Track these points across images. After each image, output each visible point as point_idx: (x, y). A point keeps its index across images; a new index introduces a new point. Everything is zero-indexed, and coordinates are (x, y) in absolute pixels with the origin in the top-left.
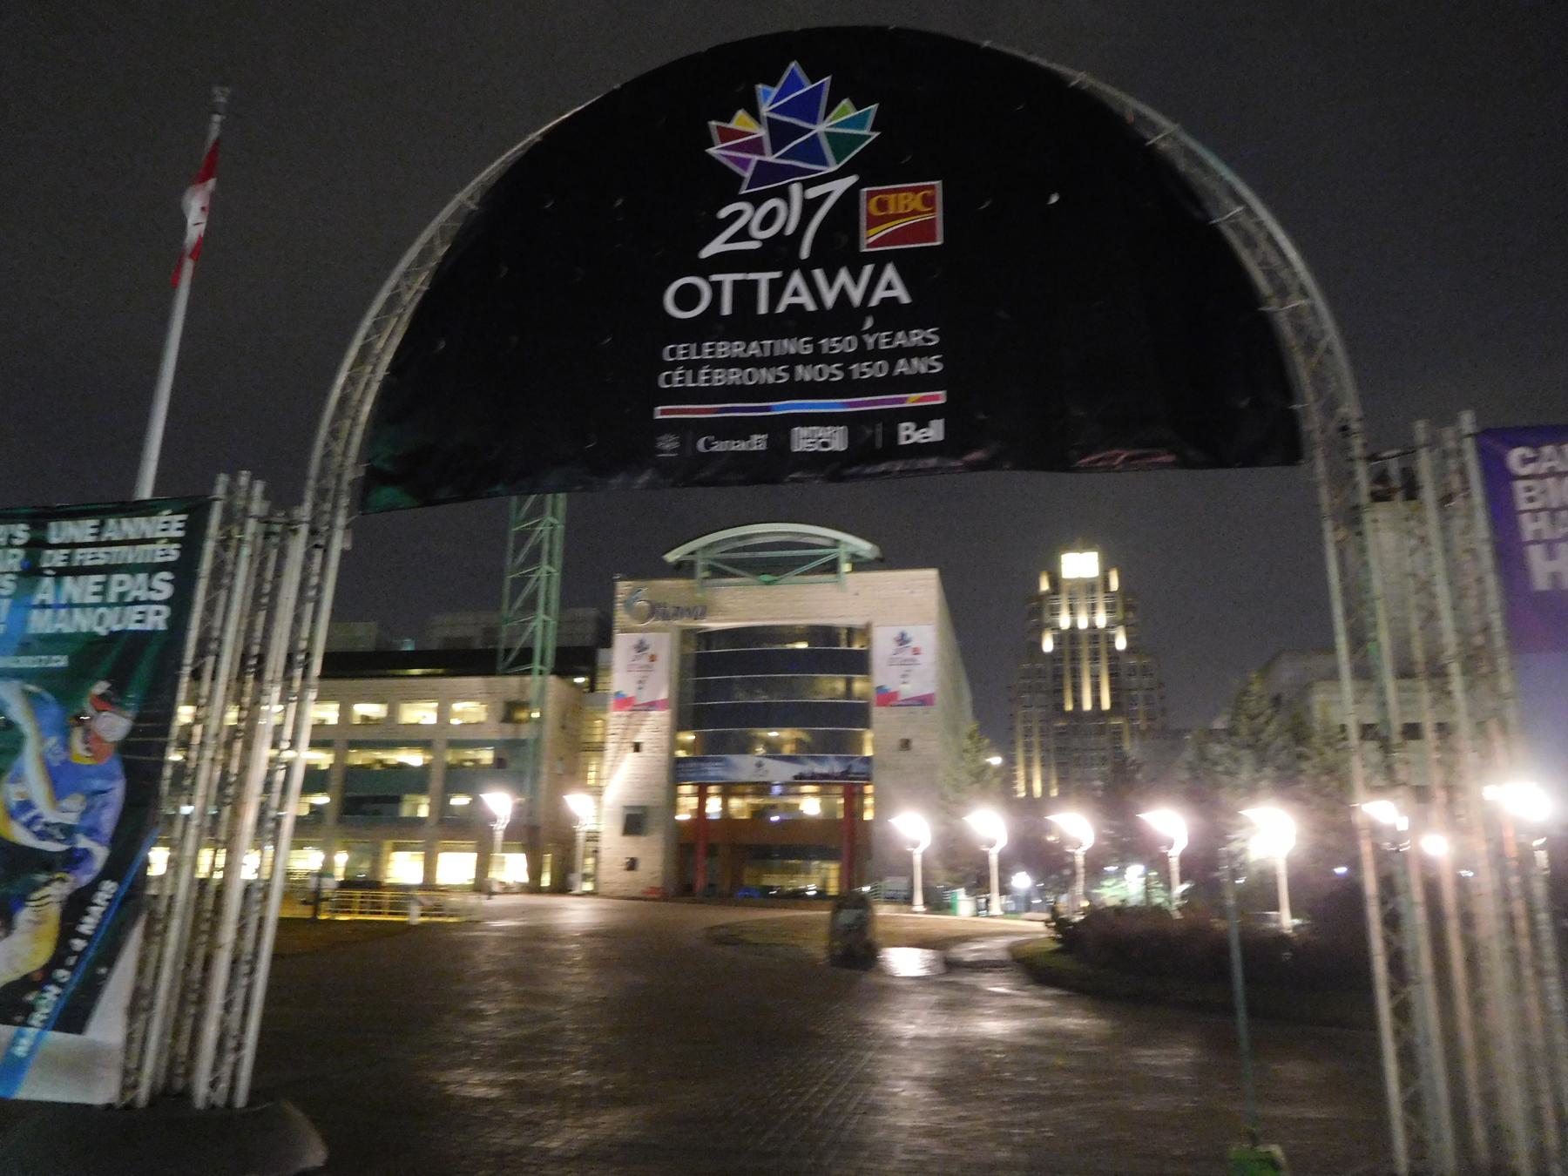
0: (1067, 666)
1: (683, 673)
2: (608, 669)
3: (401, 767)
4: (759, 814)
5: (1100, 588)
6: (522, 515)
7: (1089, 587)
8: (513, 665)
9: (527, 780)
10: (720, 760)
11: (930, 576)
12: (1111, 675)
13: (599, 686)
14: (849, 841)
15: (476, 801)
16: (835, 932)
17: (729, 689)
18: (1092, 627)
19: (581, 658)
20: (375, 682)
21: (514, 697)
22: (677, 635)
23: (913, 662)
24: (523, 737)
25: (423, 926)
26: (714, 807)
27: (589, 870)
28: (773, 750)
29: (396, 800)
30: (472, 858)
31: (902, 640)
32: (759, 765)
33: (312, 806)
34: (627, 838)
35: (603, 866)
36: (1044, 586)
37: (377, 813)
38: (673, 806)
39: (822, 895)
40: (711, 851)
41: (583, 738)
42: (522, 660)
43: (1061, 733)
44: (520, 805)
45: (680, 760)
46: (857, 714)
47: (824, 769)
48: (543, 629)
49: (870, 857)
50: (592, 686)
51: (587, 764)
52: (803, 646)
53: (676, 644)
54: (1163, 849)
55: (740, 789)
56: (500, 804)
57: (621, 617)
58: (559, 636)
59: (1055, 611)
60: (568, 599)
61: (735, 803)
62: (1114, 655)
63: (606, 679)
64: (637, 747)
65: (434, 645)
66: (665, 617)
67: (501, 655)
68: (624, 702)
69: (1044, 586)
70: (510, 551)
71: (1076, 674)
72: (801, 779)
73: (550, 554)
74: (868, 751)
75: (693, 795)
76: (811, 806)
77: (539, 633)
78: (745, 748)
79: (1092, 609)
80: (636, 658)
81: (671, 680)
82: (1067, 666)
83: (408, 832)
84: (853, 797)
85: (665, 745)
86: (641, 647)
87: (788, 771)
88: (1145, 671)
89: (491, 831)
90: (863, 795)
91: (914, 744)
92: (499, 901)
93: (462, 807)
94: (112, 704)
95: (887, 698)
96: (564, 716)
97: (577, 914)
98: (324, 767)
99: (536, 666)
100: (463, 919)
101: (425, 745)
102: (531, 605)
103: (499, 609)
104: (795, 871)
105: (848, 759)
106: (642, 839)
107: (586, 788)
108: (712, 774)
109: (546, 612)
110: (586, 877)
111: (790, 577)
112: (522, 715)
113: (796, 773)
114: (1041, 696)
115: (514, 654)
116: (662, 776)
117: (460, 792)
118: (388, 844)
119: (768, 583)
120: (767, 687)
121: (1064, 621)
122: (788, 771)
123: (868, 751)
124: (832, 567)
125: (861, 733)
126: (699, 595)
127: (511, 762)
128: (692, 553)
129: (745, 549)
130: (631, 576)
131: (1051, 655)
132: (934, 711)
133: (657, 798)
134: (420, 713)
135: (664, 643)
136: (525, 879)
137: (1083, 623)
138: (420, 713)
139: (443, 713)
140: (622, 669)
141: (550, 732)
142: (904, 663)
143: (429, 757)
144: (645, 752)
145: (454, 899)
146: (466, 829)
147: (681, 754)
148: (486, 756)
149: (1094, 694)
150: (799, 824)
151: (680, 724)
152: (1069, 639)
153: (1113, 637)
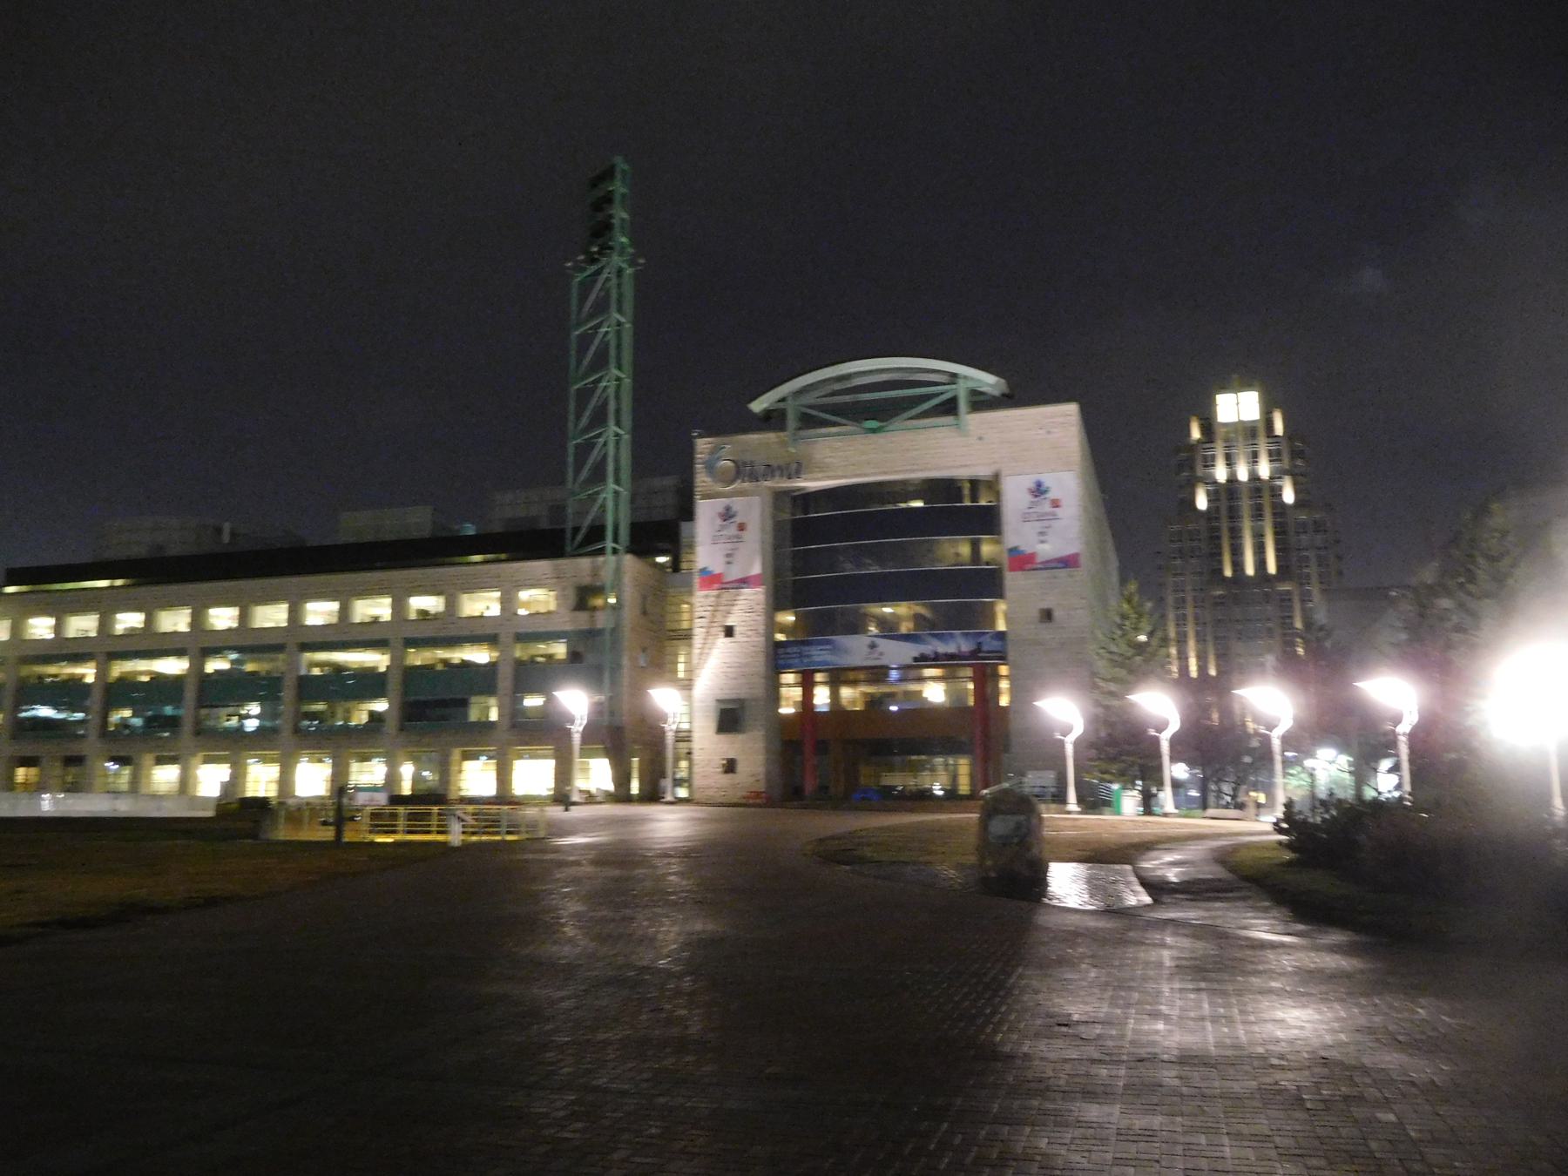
0: (1224, 525)
1: (777, 547)
2: (691, 546)
3: (466, 665)
4: (874, 703)
6: (583, 369)
7: (1249, 431)
8: (581, 545)
9: (607, 675)
10: (828, 642)
11: (1069, 412)
12: (1276, 533)
13: (684, 565)
14: (983, 731)
15: (550, 700)
16: (986, 845)
17: (834, 559)
18: (1254, 477)
19: (660, 534)
21: (587, 581)
22: (769, 499)
23: (1055, 517)
24: (599, 626)
25: (466, 848)
26: (822, 697)
27: (682, 774)
28: (889, 629)
29: (464, 703)
30: (550, 764)
31: (1039, 490)
32: (873, 646)
33: (372, 714)
34: (722, 737)
35: (696, 769)
36: (1196, 434)
37: (444, 718)
38: (774, 698)
39: (952, 795)
40: (821, 747)
41: (670, 626)
43: (1219, 603)
44: (599, 704)
45: (779, 644)
46: (987, 582)
47: (950, 648)
48: (614, 501)
49: (1006, 748)
50: (675, 566)
51: (676, 655)
52: (919, 504)
53: (769, 510)
54: (1152, 732)
55: (851, 675)
56: (576, 702)
57: (702, 480)
58: (634, 509)
59: (1209, 462)
60: (642, 467)
61: (846, 693)
62: (1280, 508)
63: (691, 557)
65: (497, 528)
66: (754, 477)
67: (569, 535)
69: (1196, 434)
70: (572, 417)
71: (1236, 534)
72: (924, 660)
73: (618, 411)
74: (1001, 626)
76: (935, 693)
77: (610, 505)
78: (856, 627)
79: (1254, 457)
80: (722, 528)
82: (1224, 525)
83: (477, 738)
84: (986, 680)
85: (762, 629)
86: (727, 515)
87: (906, 652)
88: (1318, 527)
89: (568, 733)
90: (996, 677)
91: (1057, 614)
92: (576, 812)
93: (536, 708)
95: (1022, 561)
96: (644, 598)
97: (668, 825)
98: (382, 669)
99: (609, 544)
100: (524, 836)
101: (491, 640)
102: (598, 475)
103: (563, 482)
104: (915, 768)
106: (740, 737)
107: (674, 680)
108: (817, 659)
109: (617, 481)
110: (678, 783)
111: (897, 423)
112: (599, 602)
113: (916, 654)
115: (583, 531)
117: (533, 691)
118: (456, 753)
119: (874, 431)
120: (877, 554)
121: (1221, 473)
122: (906, 652)
123: (1001, 626)
124: (949, 408)
125: (992, 605)
127: (589, 655)
128: (783, 400)
129: (834, 394)
130: (709, 432)
132: (1081, 574)
133: (759, 691)
134: (483, 604)
135: (753, 508)
136: (610, 787)
137: (1243, 474)
138: (483, 604)
139: (508, 602)
141: (629, 615)
142: (1041, 518)
143: (495, 654)
144: (738, 637)
145: (531, 812)
146: (543, 733)
147: (780, 637)
148: (560, 650)
149: (1258, 555)
150: (924, 714)
151: (778, 602)
152: (1227, 493)
153: (1280, 488)
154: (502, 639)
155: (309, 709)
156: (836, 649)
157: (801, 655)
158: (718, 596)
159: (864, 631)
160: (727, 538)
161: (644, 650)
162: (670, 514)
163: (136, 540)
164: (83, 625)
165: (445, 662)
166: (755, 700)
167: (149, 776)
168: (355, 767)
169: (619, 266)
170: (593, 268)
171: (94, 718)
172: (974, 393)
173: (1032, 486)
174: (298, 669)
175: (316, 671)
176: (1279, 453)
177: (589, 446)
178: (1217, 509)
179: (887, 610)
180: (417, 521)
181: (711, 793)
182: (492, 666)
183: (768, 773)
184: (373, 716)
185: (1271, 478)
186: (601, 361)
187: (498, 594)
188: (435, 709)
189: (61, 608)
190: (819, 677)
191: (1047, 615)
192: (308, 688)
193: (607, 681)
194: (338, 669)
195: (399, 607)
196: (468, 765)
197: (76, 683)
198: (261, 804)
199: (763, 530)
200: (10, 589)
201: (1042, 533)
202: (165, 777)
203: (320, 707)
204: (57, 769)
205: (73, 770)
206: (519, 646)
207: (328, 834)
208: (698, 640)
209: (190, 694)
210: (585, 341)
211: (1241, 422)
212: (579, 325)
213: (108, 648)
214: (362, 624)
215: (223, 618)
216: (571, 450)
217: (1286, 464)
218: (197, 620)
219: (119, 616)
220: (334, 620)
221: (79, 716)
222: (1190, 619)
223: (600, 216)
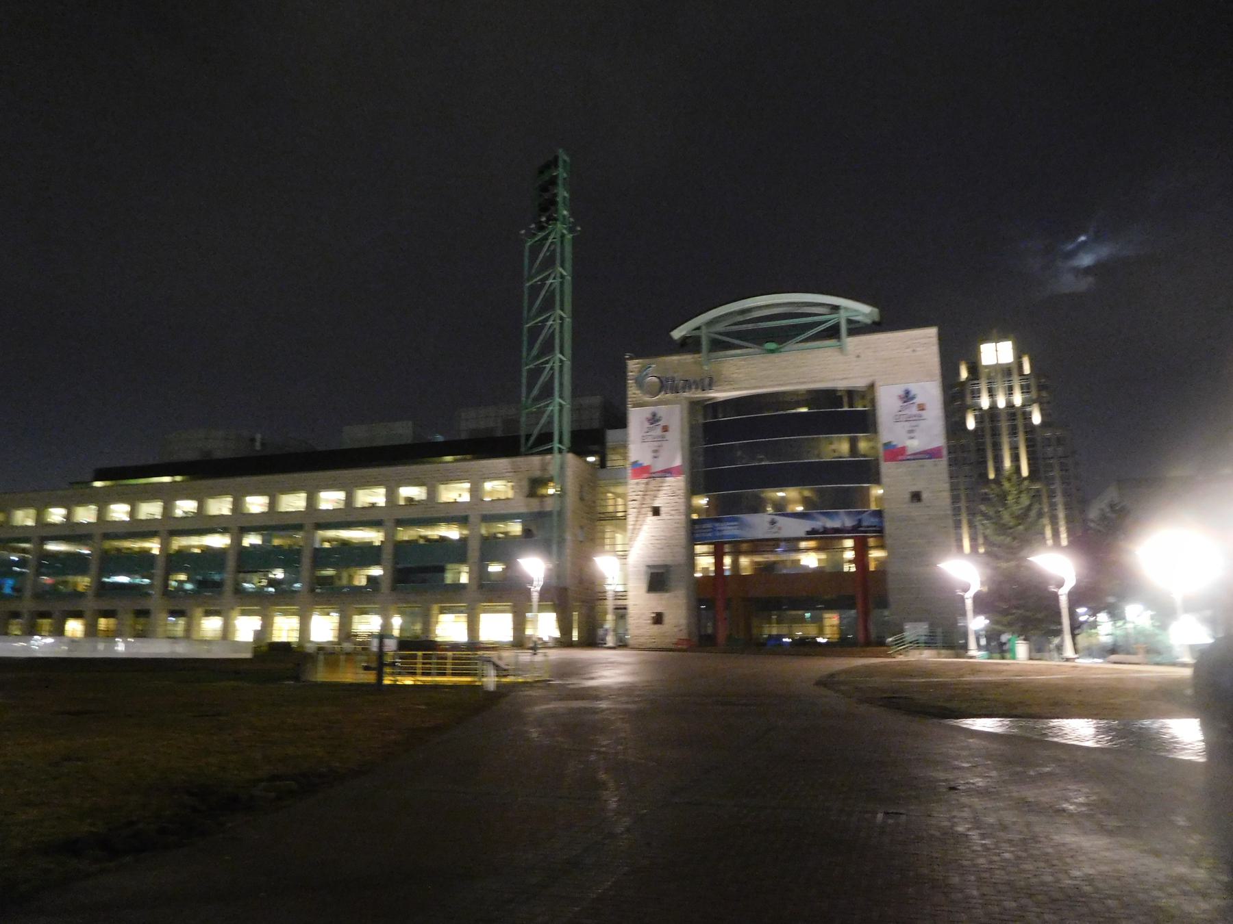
0: (988, 440)
3: (443, 540)
4: (765, 570)
5: (1015, 372)
8: (531, 448)
9: (555, 548)
12: (1028, 447)
13: (609, 464)
17: (738, 454)
18: (1010, 405)
19: (596, 435)
20: (414, 467)
21: (538, 474)
22: (686, 406)
23: (919, 418)
24: (548, 509)
28: (780, 508)
29: (442, 570)
31: (907, 397)
32: (773, 523)
34: (652, 595)
36: (964, 374)
37: (424, 581)
38: (692, 565)
42: (542, 444)
45: (694, 522)
46: (867, 471)
48: (560, 411)
50: (603, 464)
51: (604, 532)
52: (804, 410)
53: (686, 414)
54: (1052, 589)
57: (633, 392)
59: (976, 394)
61: (744, 561)
62: (1030, 429)
64: (656, 511)
66: (675, 390)
67: (523, 440)
68: (641, 470)
69: (964, 374)
71: (997, 447)
75: (708, 554)
78: (757, 507)
79: (1010, 391)
80: (650, 430)
81: (683, 448)
82: (988, 440)
83: (453, 597)
85: (682, 508)
86: (654, 419)
88: (1059, 441)
91: (924, 496)
94: (1077, 823)
95: (895, 453)
96: (581, 487)
98: (377, 543)
99: (556, 445)
102: (547, 392)
105: (859, 513)
106: (667, 595)
108: (725, 533)
111: (791, 345)
114: (967, 468)
115: (533, 439)
116: (682, 536)
118: (435, 608)
119: (772, 351)
121: (985, 403)
124: (833, 333)
126: (706, 368)
127: (541, 527)
128: (698, 328)
129: (735, 324)
131: (976, 430)
133: (681, 558)
134: (456, 493)
135: (674, 414)
136: (557, 634)
137: (1001, 403)
138: (456, 493)
139: (475, 491)
140: (637, 442)
141: (571, 500)
143: (465, 532)
144: (663, 516)
146: (509, 593)
147: (695, 516)
148: (516, 528)
151: (694, 489)
153: (1030, 413)
154: (471, 519)
155: (322, 575)
156: (742, 525)
157: (714, 530)
158: (647, 484)
159: (764, 511)
160: (653, 437)
161: (582, 527)
162: (596, 425)
163: (190, 447)
164: (151, 510)
165: (426, 538)
166: (680, 565)
167: (199, 625)
168: (356, 618)
169: (561, 232)
170: (541, 235)
171: (158, 582)
172: (849, 321)
173: (902, 393)
174: (313, 543)
175: (327, 545)
176: (1028, 387)
177: (538, 371)
178: (982, 430)
179: (781, 494)
180: (402, 431)
181: (642, 640)
182: (463, 541)
183: (689, 624)
184: (371, 579)
185: (1023, 406)
186: (548, 305)
187: (468, 485)
188: (418, 574)
189: (133, 498)
190: (727, 548)
191: (916, 497)
192: (321, 557)
193: (555, 548)
194: (345, 544)
195: (391, 495)
196: (444, 618)
197: (146, 553)
198: (286, 646)
199: (682, 432)
200: (98, 484)
201: (911, 431)
202: (211, 625)
203: (330, 572)
204: (129, 620)
205: (142, 620)
206: (483, 525)
207: (370, 677)
208: (631, 519)
209: (231, 563)
210: (535, 290)
211: (997, 365)
212: (531, 277)
213: (170, 528)
214: (363, 508)
215: (256, 504)
216: (525, 374)
217: (1034, 394)
218: (237, 506)
219: (179, 503)
220: (341, 506)
221: (147, 581)
222: (964, 510)
223: (546, 196)
